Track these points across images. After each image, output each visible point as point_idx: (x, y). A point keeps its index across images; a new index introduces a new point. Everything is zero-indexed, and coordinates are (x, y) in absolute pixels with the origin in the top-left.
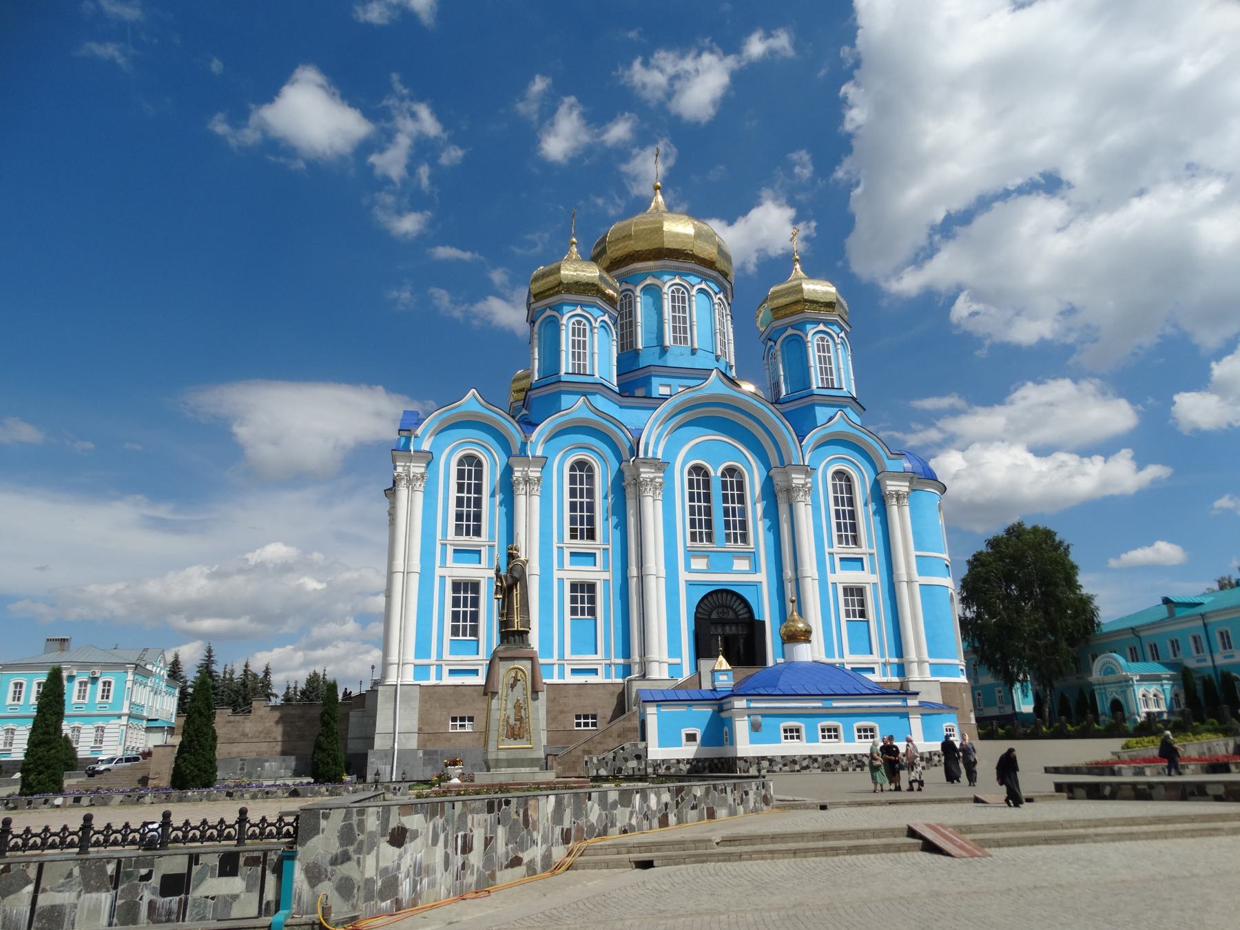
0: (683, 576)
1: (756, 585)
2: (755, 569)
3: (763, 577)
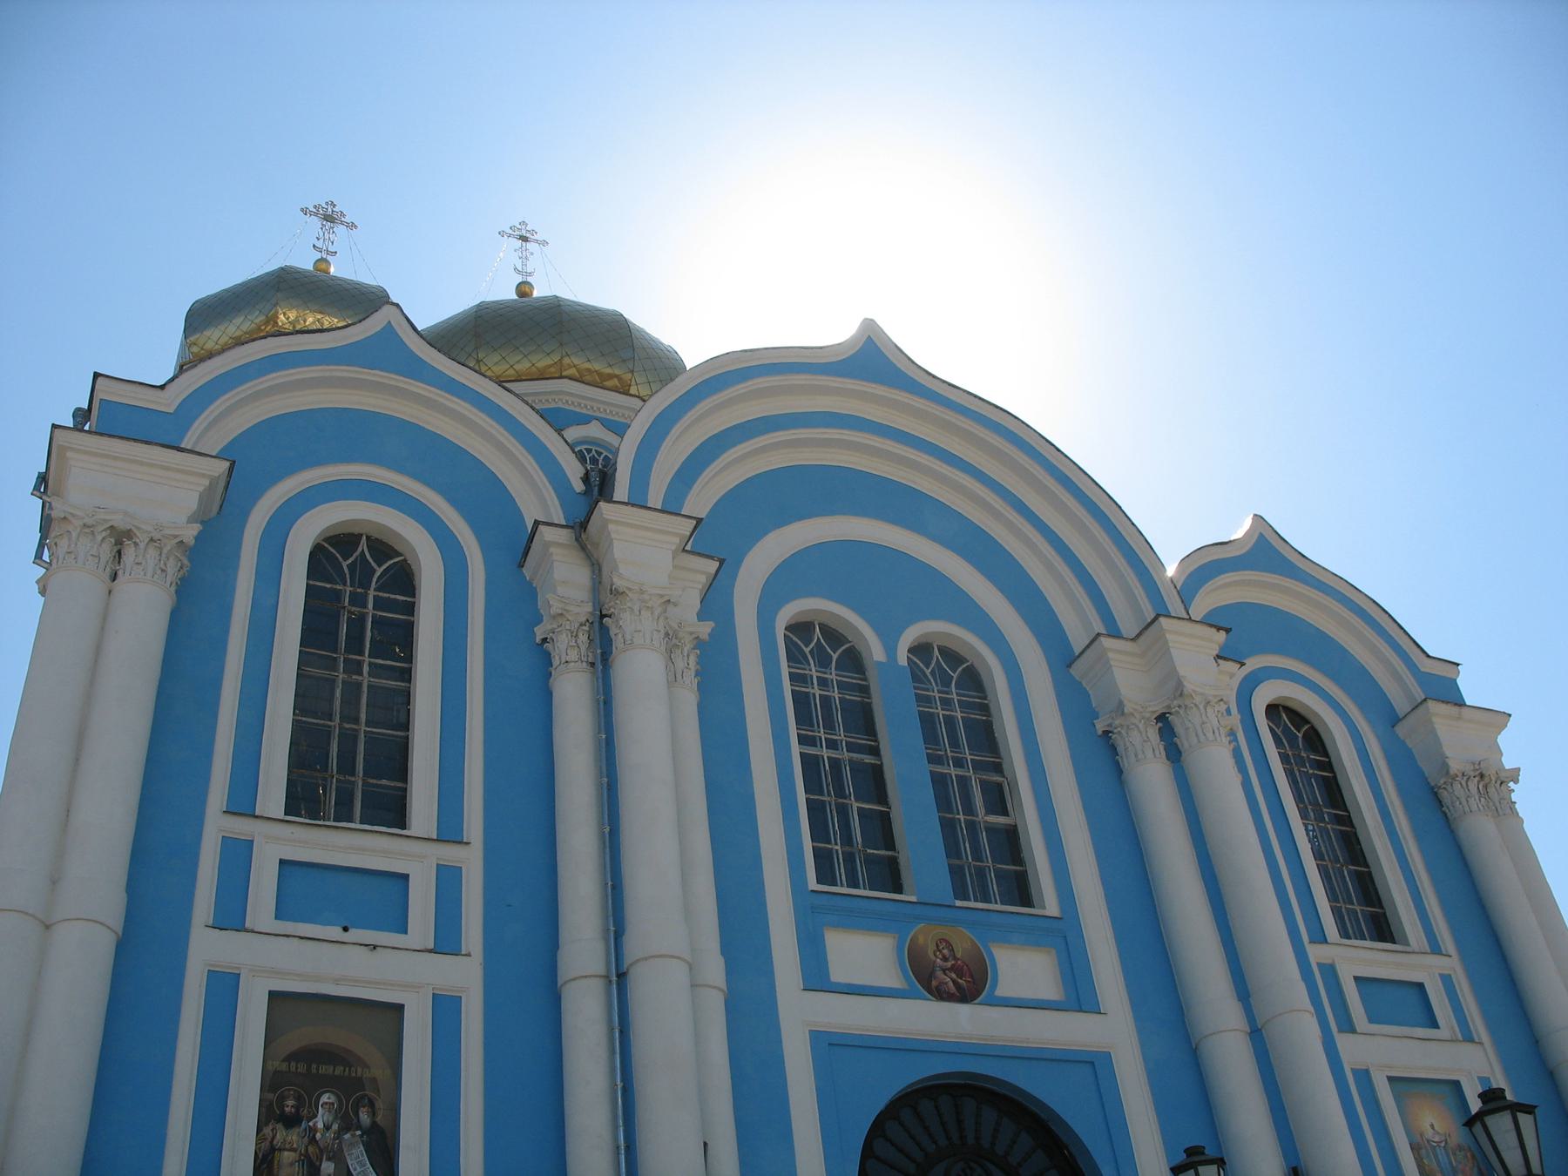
0: (800, 1014)
1: (1095, 1065)
2: (1079, 995)
3: (1113, 1030)
